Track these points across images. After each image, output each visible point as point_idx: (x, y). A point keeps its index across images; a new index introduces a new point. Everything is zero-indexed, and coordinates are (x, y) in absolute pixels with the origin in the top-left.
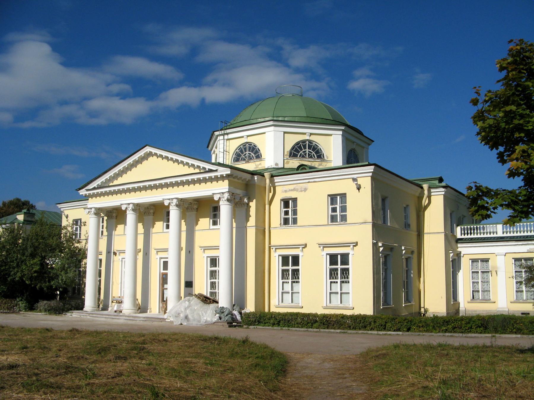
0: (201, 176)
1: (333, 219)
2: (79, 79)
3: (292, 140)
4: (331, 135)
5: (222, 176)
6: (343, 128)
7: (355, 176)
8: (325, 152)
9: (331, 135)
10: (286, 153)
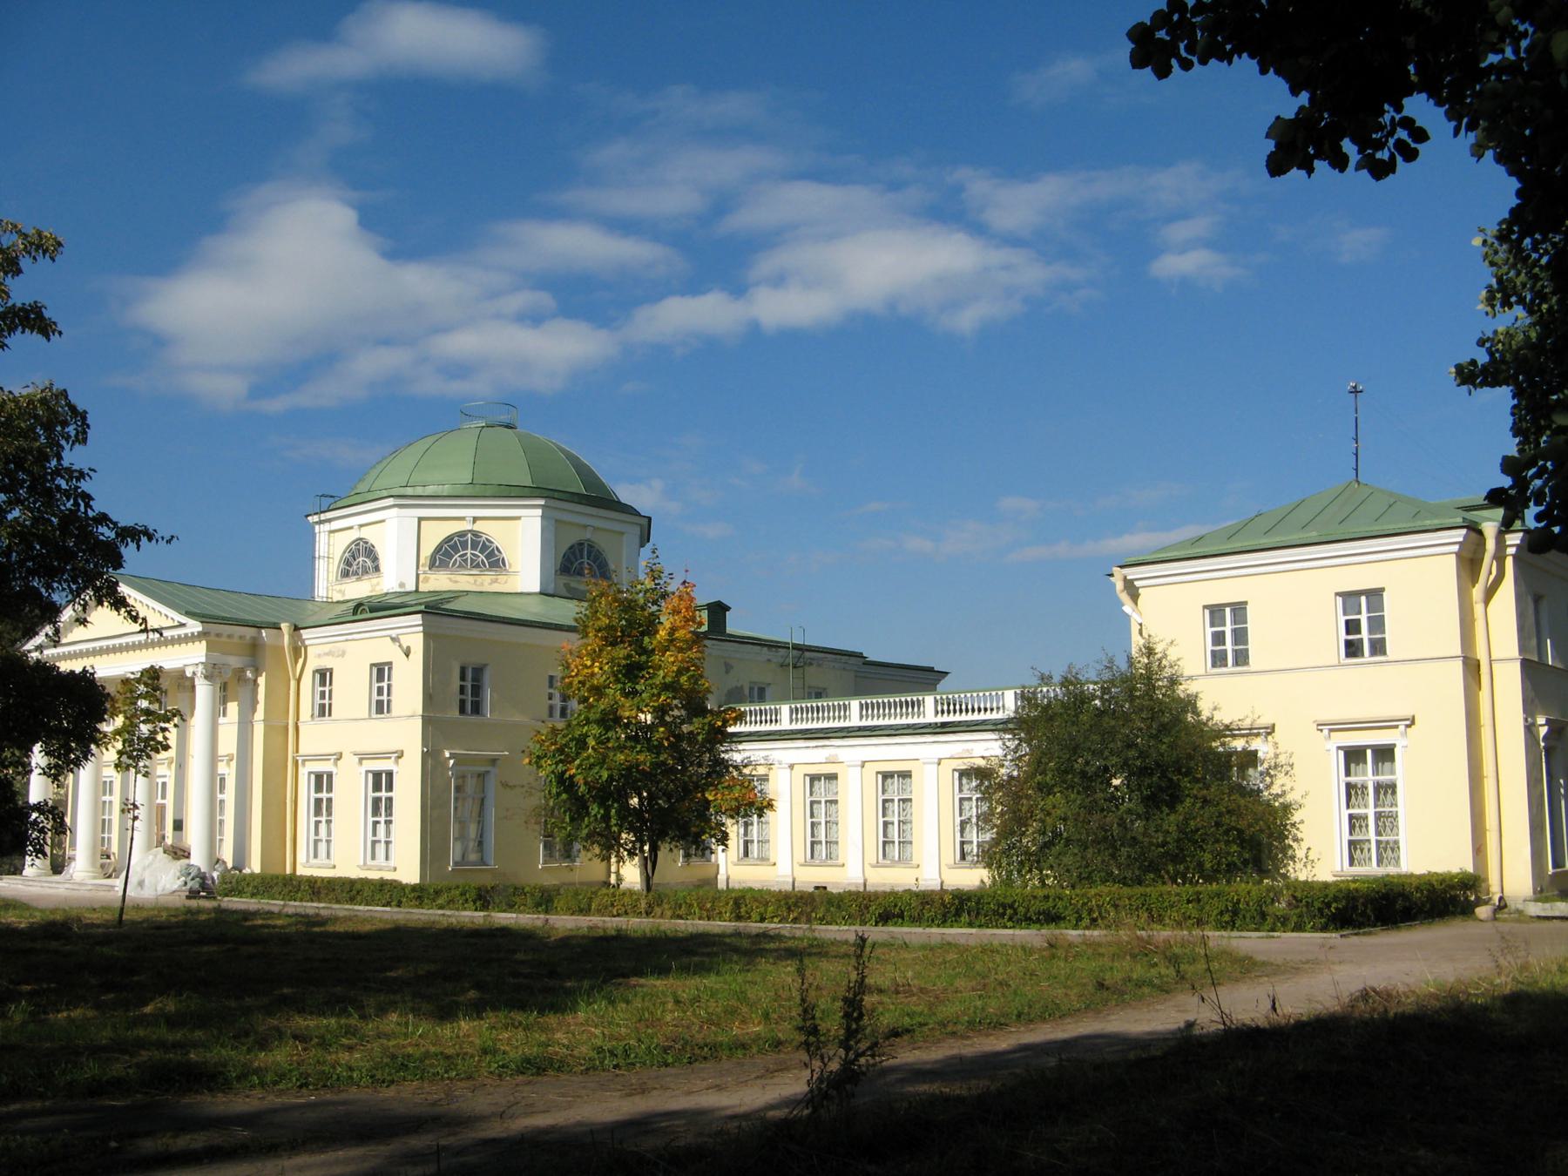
1: (1353, 649)
2: (421, 282)
3: (435, 534)
4: (518, 518)
6: (542, 502)
7: (393, 633)
9: (518, 518)
10: (422, 561)
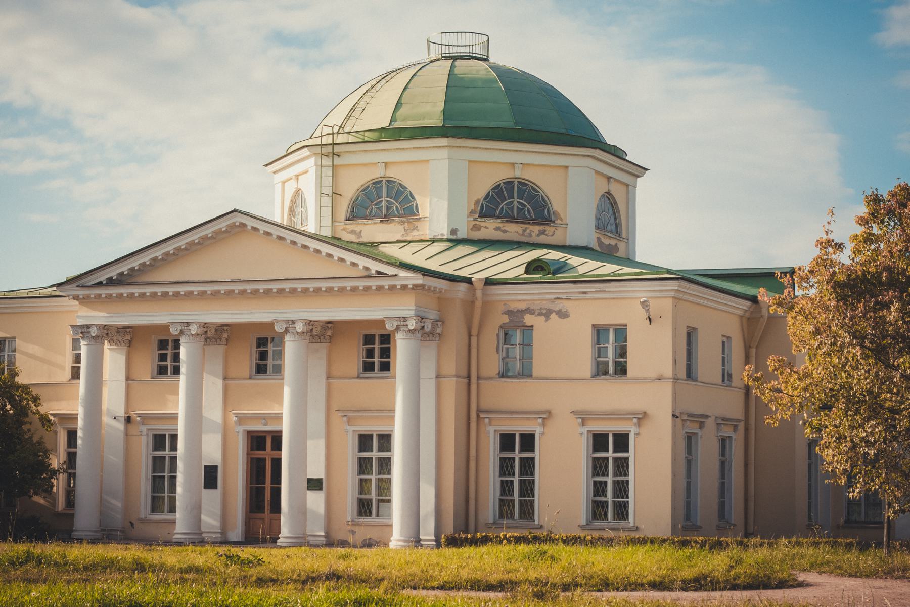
0: (361, 284)
5: (404, 287)
8: (556, 205)
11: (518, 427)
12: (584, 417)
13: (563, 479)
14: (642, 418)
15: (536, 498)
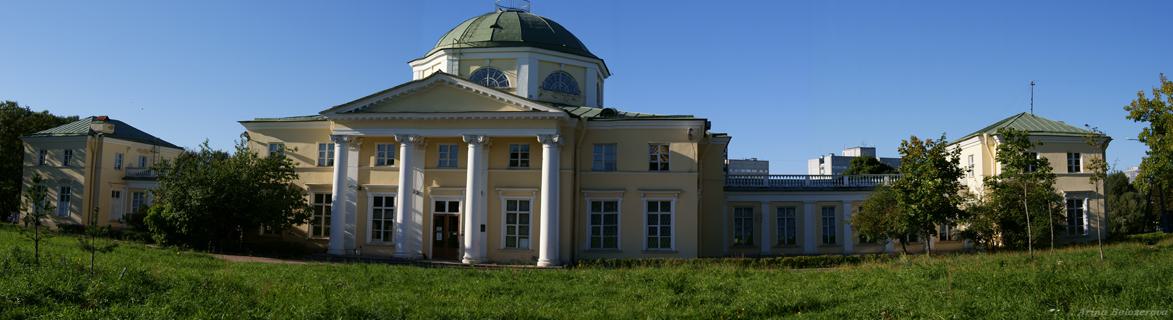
11: (603, 198)
12: (645, 191)
13: (632, 224)
14: (680, 192)
15: (619, 236)
